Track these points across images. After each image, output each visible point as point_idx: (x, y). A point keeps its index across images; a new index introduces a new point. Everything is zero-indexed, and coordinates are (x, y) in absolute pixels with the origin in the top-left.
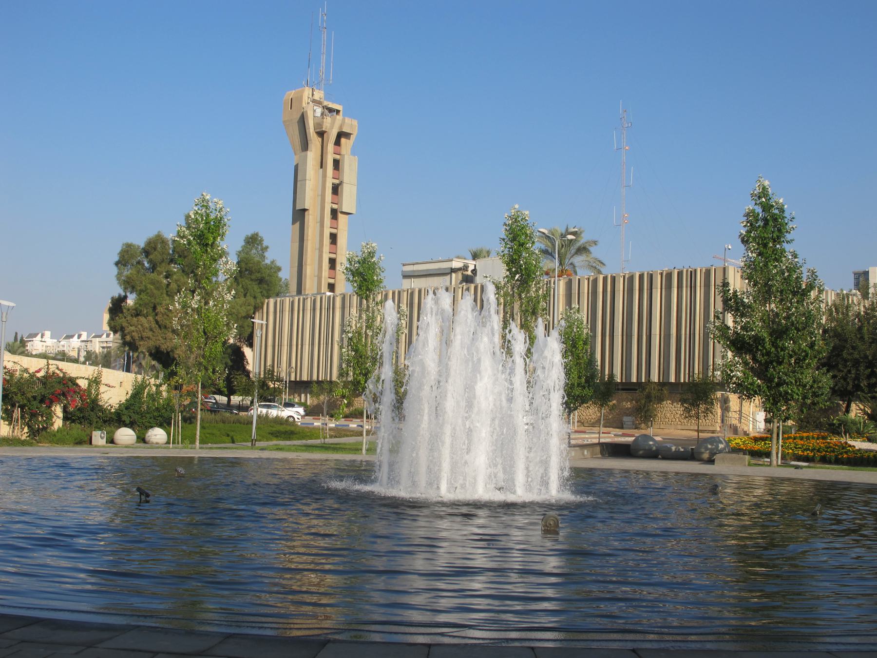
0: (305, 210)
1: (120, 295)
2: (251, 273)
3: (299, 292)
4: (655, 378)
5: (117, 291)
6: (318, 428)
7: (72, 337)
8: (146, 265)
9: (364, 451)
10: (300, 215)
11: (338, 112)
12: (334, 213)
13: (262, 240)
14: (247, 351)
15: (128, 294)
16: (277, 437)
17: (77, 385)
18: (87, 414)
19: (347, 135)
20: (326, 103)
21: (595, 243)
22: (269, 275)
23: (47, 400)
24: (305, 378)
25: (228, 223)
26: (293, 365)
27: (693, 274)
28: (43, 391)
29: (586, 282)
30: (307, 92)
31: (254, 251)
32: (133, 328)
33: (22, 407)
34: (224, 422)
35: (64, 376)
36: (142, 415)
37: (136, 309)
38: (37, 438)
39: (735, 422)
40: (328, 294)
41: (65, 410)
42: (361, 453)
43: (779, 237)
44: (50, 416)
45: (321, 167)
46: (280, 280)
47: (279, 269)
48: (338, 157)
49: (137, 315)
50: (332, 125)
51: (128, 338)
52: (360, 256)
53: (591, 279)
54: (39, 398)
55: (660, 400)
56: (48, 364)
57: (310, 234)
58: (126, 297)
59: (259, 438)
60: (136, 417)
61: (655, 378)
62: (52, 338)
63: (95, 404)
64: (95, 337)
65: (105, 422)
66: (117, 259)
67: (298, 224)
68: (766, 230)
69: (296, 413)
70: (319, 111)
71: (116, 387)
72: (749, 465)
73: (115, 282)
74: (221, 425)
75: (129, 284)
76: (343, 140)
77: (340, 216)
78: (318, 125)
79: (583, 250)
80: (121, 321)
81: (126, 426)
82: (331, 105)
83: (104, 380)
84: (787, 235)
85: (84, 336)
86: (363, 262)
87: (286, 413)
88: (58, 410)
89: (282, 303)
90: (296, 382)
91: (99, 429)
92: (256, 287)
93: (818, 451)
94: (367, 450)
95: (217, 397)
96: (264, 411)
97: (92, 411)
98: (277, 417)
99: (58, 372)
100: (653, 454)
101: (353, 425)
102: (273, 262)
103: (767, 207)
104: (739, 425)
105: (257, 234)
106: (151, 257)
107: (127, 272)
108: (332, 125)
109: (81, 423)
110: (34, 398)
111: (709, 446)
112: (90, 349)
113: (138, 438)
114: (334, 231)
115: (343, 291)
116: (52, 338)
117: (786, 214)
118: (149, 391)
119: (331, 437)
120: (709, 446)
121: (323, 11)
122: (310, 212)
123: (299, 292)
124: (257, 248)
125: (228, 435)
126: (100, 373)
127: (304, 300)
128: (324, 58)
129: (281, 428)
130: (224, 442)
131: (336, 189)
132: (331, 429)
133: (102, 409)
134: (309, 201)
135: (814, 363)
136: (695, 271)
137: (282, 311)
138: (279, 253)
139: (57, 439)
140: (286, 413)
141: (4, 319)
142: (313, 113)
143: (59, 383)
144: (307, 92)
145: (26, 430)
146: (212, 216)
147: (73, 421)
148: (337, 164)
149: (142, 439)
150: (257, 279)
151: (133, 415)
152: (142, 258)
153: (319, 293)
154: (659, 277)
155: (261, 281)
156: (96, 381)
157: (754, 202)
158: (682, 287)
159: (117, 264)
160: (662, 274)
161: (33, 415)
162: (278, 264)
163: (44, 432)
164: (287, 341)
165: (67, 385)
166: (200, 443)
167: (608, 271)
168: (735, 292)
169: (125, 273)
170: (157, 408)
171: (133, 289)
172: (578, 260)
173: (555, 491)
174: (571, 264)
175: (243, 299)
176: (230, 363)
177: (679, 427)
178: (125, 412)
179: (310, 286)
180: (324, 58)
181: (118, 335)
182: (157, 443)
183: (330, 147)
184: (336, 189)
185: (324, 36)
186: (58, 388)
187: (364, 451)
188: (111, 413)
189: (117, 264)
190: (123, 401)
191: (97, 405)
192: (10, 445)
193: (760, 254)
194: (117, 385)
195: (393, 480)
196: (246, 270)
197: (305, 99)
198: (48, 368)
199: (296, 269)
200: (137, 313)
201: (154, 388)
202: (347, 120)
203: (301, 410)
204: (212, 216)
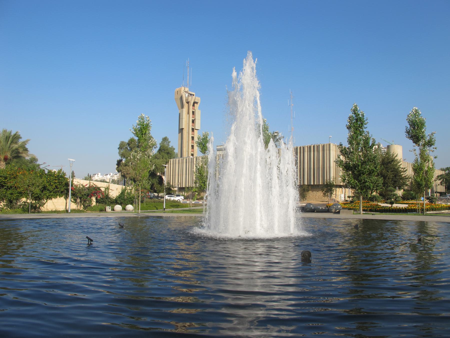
0: (183, 129)
2: (165, 150)
3: (181, 156)
5: (119, 158)
6: (187, 204)
10: (181, 130)
11: (193, 95)
12: (193, 130)
14: (164, 177)
19: (197, 103)
23: (90, 195)
26: (180, 182)
27: (318, 147)
28: (88, 192)
30: (183, 88)
31: (165, 143)
33: (80, 198)
34: (154, 202)
36: (125, 200)
39: (334, 198)
40: (191, 157)
41: (96, 199)
44: (91, 201)
47: (174, 149)
48: (194, 110)
49: (126, 166)
51: (123, 174)
52: (202, 137)
58: (122, 160)
60: (123, 201)
63: (107, 197)
65: (111, 203)
66: (118, 147)
68: (357, 124)
69: (180, 199)
70: (187, 95)
71: (115, 191)
74: (153, 203)
75: (123, 155)
76: (195, 105)
77: (195, 130)
80: (120, 168)
81: (119, 204)
82: (191, 93)
85: (112, 175)
86: (203, 139)
87: (177, 198)
88: (94, 199)
89: (176, 161)
90: (181, 188)
91: (109, 205)
95: (155, 194)
103: (357, 115)
110: (85, 195)
114: (193, 136)
117: (365, 118)
119: (193, 207)
123: (181, 156)
126: (109, 185)
129: (175, 204)
131: (193, 121)
132: (192, 204)
133: (110, 198)
135: (376, 174)
137: (175, 163)
138: (174, 144)
139: (93, 209)
140: (177, 198)
142: (185, 96)
144: (183, 88)
145: (82, 206)
146: (145, 123)
147: (100, 203)
148: (193, 113)
149: (124, 209)
150: (166, 152)
152: (127, 146)
155: (168, 153)
156: (107, 188)
159: (119, 148)
161: (85, 201)
162: (174, 147)
164: (177, 174)
168: (345, 148)
169: (122, 151)
173: (294, 230)
179: (185, 154)
181: (120, 173)
183: (191, 107)
184: (193, 121)
189: (119, 148)
193: (355, 133)
194: (115, 190)
197: (182, 91)
200: (126, 165)
202: (197, 98)
203: (183, 197)
204: (145, 123)
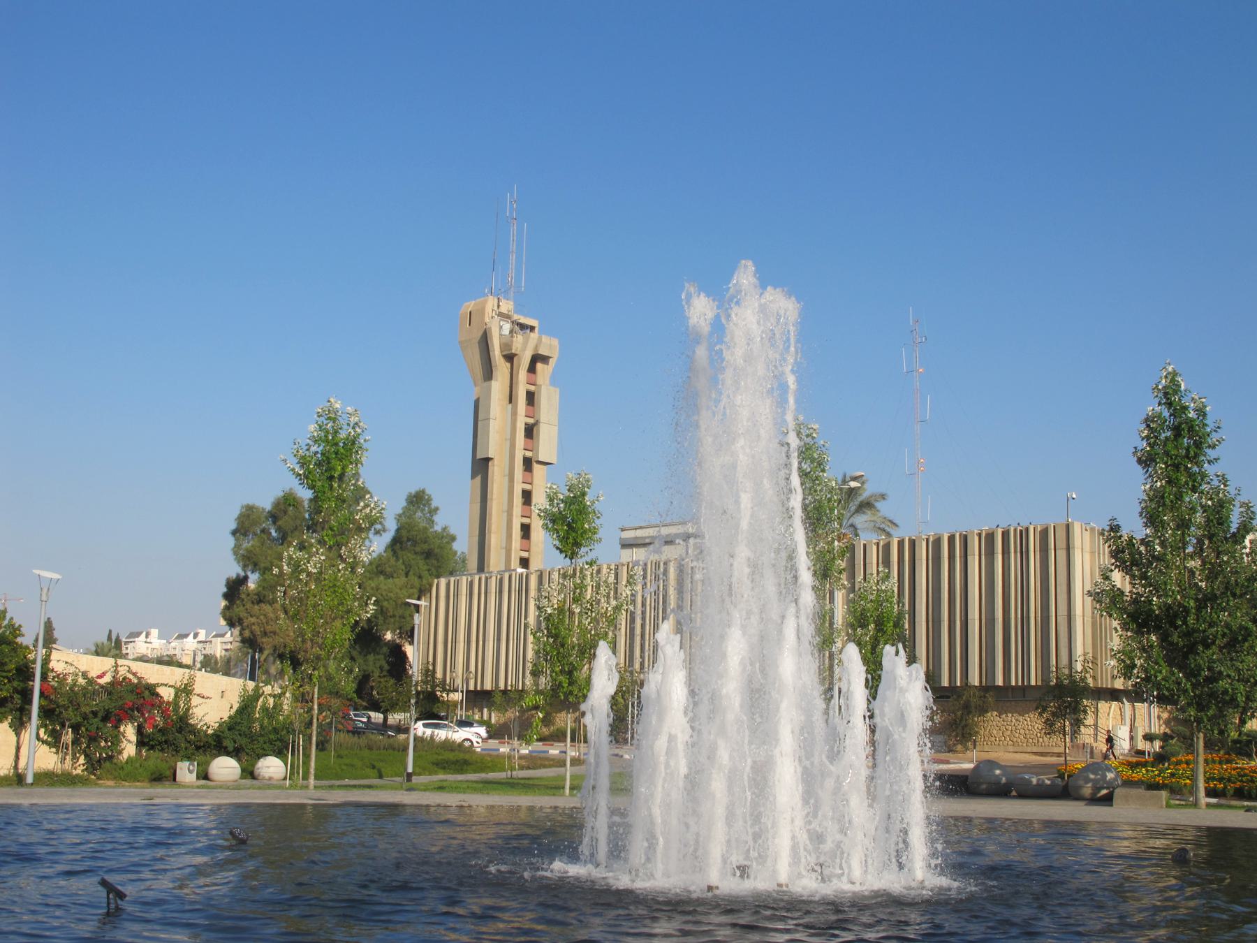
0: (488, 460)
1: (238, 576)
2: (415, 543)
3: (481, 568)
4: (975, 680)
5: (235, 570)
6: (502, 756)
7: (186, 636)
8: (274, 534)
9: (567, 791)
10: (481, 466)
11: (532, 328)
12: (528, 464)
13: (429, 499)
14: (409, 650)
15: (249, 573)
16: (444, 768)
17: (158, 695)
18: (171, 737)
19: (545, 359)
20: (516, 317)
21: (883, 497)
22: (440, 547)
24: (488, 687)
25: (365, 446)
26: (472, 668)
29: (875, 548)
30: (491, 302)
31: (419, 514)
32: (253, 620)
33: (76, 728)
34: (370, 748)
35: (140, 682)
36: (252, 738)
37: (258, 594)
38: (98, 772)
40: (520, 570)
41: (140, 731)
42: (563, 795)
43: (1196, 455)
44: (117, 739)
45: (510, 402)
46: (456, 553)
47: (453, 539)
48: (532, 388)
50: (525, 347)
53: (882, 543)
54: (100, 715)
55: (983, 711)
56: (116, 666)
57: (495, 491)
59: (418, 770)
60: (243, 741)
61: (975, 680)
62: (160, 637)
63: (182, 724)
64: (216, 636)
65: (198, 748)
66: (233, 526)
67: (479, 478)
69: (474, 735)
70: (507, 327)
71: (215, 700)
72: (1168, 806)
73: (231, 558)
74: (366, 753)
75: (249, 560)
76: (539, 366)
77: (536, 466)
78: (506, 346)
79: (866, 505)
80: (239, 610)
81: (228, 754)
82: (523, 320)
83: (198, 688)
84: (1209, 451)
85: (202, 635)
87: (460, 735)
88: (129, 731)
89: (457, 584)
90: (476, 692)
92: (421, 563)
93: (1229, 780)
94: (572, 788)
95: (372, 714)
96: (429, 731)
97: (180, 732)
98: (447, 740)
99: (131, 676)
100: (1001, 791)
101: (554, 751)
102: (444, 529)
104: (1094, 745)
105: (423, 491)
106: (280, 523)
107: (247, 544)
108: (525, 347)
109: (162, 750)
110: (95, 714)
111: (1092, 776)
112: (208, 651)
113: (243, 770)
114: (527, 487)
115: (541, 567)
116: (160, 637)
118: (264, 703)
119: (522, 768)
120: (1092, 776)
121: (512, 196)
122: (496, 462)
123: (481, 568)
124: (422, 511)
125: (374, 767)
127: (487, 579)
128: (513, 259)
129: (451, 756)
130: (368, 777)
131: (530, 431)
133: (193, 730)
134: (494, 447)
136: (1027, 529)
137: (457, 595)
138: (453, 518)
139: (126, 773)
140: (460, 735)
141: (44, 598)
142: (500, 331)
143: (132, 692)
144: (491, 302)
145: (82, 760)
146: (343, 434)
147: (152, 748)
148: (531, 398)
151: (238, 738)
153: (508, 569)
154: (977, 538)
155: (428, 555)
156: (185, 691)
157: (1157, 400)
158: (1009, 553)
159: (234, 533)
160: (980, 535)
161: (93, 739)
162: (452, 531)
163: (108, 764)
164: (464, 636)
165: (144, 694)
166: (316, 778)
167: (903, 532)
168: (1131, 538)
170: (275, 729)
171: (255, 566)
172: (860, 520)
174: (852, 525)
175: (404, 579)
176: (386, 667)
177: (1011, 749)
178: (227, 733)
179: (495, 561)
180: (513, 259)
181: (236, 631)
182: (270, 779)
183: (522, 375)
184: (530, 431)
185: (514, 228)
186: (132, 699)
187: (567, 791)
188: (206, 735)
189: (234, 533)
190: (226, 718)
191: (188, 725)
192: (52, 785)
193: (1169, 482)
195: (618, 850)
196: (409, 540)
198: (116, 671)
199: (476, 539)
200: (260, 599)
201: (271, 701)
202: (545, 339)
203: (482, 731)
204: (343, 434)
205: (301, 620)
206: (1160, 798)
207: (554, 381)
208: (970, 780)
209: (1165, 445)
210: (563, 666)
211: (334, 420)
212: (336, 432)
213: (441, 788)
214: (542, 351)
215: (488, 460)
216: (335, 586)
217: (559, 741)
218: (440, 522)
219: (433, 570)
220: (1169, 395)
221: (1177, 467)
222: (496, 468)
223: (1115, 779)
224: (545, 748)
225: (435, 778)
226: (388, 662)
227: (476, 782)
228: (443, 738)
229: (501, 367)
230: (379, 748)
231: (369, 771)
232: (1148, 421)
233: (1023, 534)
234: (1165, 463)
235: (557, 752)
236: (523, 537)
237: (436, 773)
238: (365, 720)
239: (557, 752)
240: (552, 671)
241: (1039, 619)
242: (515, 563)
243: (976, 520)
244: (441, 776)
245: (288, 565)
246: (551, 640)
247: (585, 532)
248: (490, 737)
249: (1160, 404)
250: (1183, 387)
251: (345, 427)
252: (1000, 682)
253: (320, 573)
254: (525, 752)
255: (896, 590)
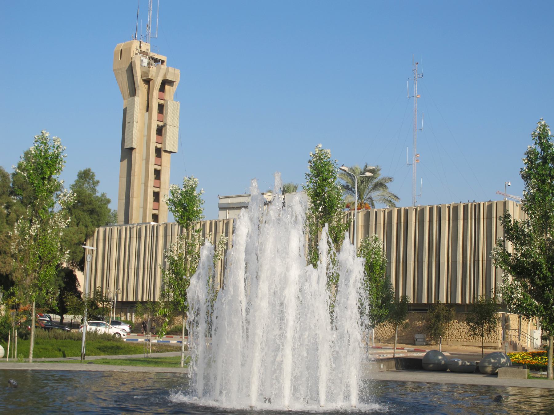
0: (132, 149)
3: (126, 221)
6: (141, 344)
9: (182, 365)
10: (127, 153)
11: (163, 62)
12: (159, 152)
13: (93, 175)
14: (79, 274)
16: (104, 351)
19: (171, 83)
20: (152, 54)
21: (390, 179)
25: (64, 159)
26: (120, 287)
29: (382, 214)
30: (135, 44)
31: (86, 185)
34: (56, 338)
40: (153, 223)
45: (147, 111)
46: (110, 211)
47: (109, 201)
48: (162, 102)
50: (158, 74)
53: (387, 211)
55: (448, 319)
67: (125, 161)
69: (122, 330)
70: (146, 61)
72: (529, 377)
74: (54, 341)
76: (167, 87)
82: (157, 56)
89: (111, 231)
90: (122, 302)
92: (87, 217)
95: (52, 315)
96: (93, 328)
98: (105, 334)
100: (442, 368)
101: (173, 341)
102: (103, 195)
104: (518, 342)
105: (89, 170)
108: (158, 74)
111: (493, 361)
114: (158, 168)
119: (153, 351)
120: (493, 361)
122: (137, 150)
123: (126, 221)
124: (88, 183)
125: (60, 350)
127: (130, 228)
129: (108, 344)
130: (57, 356)
131: (160, 131)
134: (136, 140)
136: (479, 204)
137: (111, 239)
138: (109, 187)
142: (141, 63)
144: (135, 44)
146: (50, 152)
148: (161, 108)
153: (144, 222)
154: (447, 210)
155: (92, 212)
157: (534, 141)
158: (467, 219)
160: (449, 207)
162: (108, 197)
167: (401, 204)
172: (376, 195)
174: (369, 198)
175: (76, 228)
177: (465, 344)
179: (136, 216)
183: (156, 93)
184: (160, 131)
187: (182, 365)
202: (171, 70)
203: (127, 328)
204: (50, 152)
205: (25, 263)
206: (524, 373)
207: (176, 98)
208: (423, 361)
209: (537, 168)
210: (181, 291)
211: (45, 144)
212: (46, 151)
213: (107, 363)
214: (169, 78)
215: (132, 149)
216: (45, 243)
217: (177, 335)
218: (100, 191)
219: (95, 222)
220: (542, 137)
221: (543, 182)
222: (137, 154)
223: (506, 363)
224: (168, 339)
225: (98, 357)
226: (64, 282)
227: (126, 360)
228: (103, 332)
229: (142, 88)
230: (62, 338)
231: (57, 353)
232: (528, 153)
233: (477, 207)
234: (537, 179)
235: (175, 342)
236: (155, 201)
237: (99, 354)
238: (48, 319)
239: (175, 342)
240: (174, 294)
241: (485, 262)
242: (149, 218)
243: (447, 200)
244: (103, 356)
245: (18, 230)
246: (174, 276)
247: (194, 212)
248: (132, 331)
249: (536, 144)
250: (550, 134)
251: (52, 148)
252: (459, 301)
253: (37, 235)
254: (155, 341)
255: (382, 247)
